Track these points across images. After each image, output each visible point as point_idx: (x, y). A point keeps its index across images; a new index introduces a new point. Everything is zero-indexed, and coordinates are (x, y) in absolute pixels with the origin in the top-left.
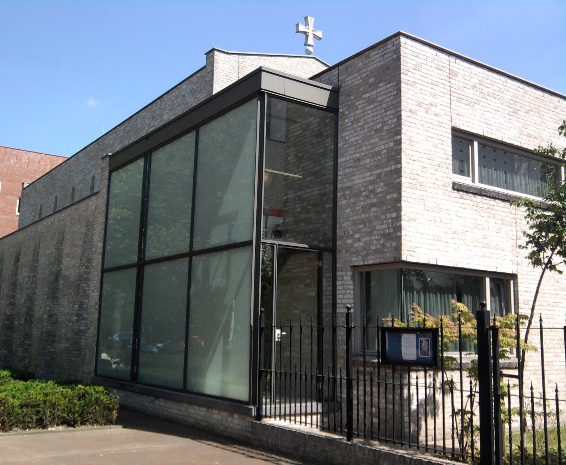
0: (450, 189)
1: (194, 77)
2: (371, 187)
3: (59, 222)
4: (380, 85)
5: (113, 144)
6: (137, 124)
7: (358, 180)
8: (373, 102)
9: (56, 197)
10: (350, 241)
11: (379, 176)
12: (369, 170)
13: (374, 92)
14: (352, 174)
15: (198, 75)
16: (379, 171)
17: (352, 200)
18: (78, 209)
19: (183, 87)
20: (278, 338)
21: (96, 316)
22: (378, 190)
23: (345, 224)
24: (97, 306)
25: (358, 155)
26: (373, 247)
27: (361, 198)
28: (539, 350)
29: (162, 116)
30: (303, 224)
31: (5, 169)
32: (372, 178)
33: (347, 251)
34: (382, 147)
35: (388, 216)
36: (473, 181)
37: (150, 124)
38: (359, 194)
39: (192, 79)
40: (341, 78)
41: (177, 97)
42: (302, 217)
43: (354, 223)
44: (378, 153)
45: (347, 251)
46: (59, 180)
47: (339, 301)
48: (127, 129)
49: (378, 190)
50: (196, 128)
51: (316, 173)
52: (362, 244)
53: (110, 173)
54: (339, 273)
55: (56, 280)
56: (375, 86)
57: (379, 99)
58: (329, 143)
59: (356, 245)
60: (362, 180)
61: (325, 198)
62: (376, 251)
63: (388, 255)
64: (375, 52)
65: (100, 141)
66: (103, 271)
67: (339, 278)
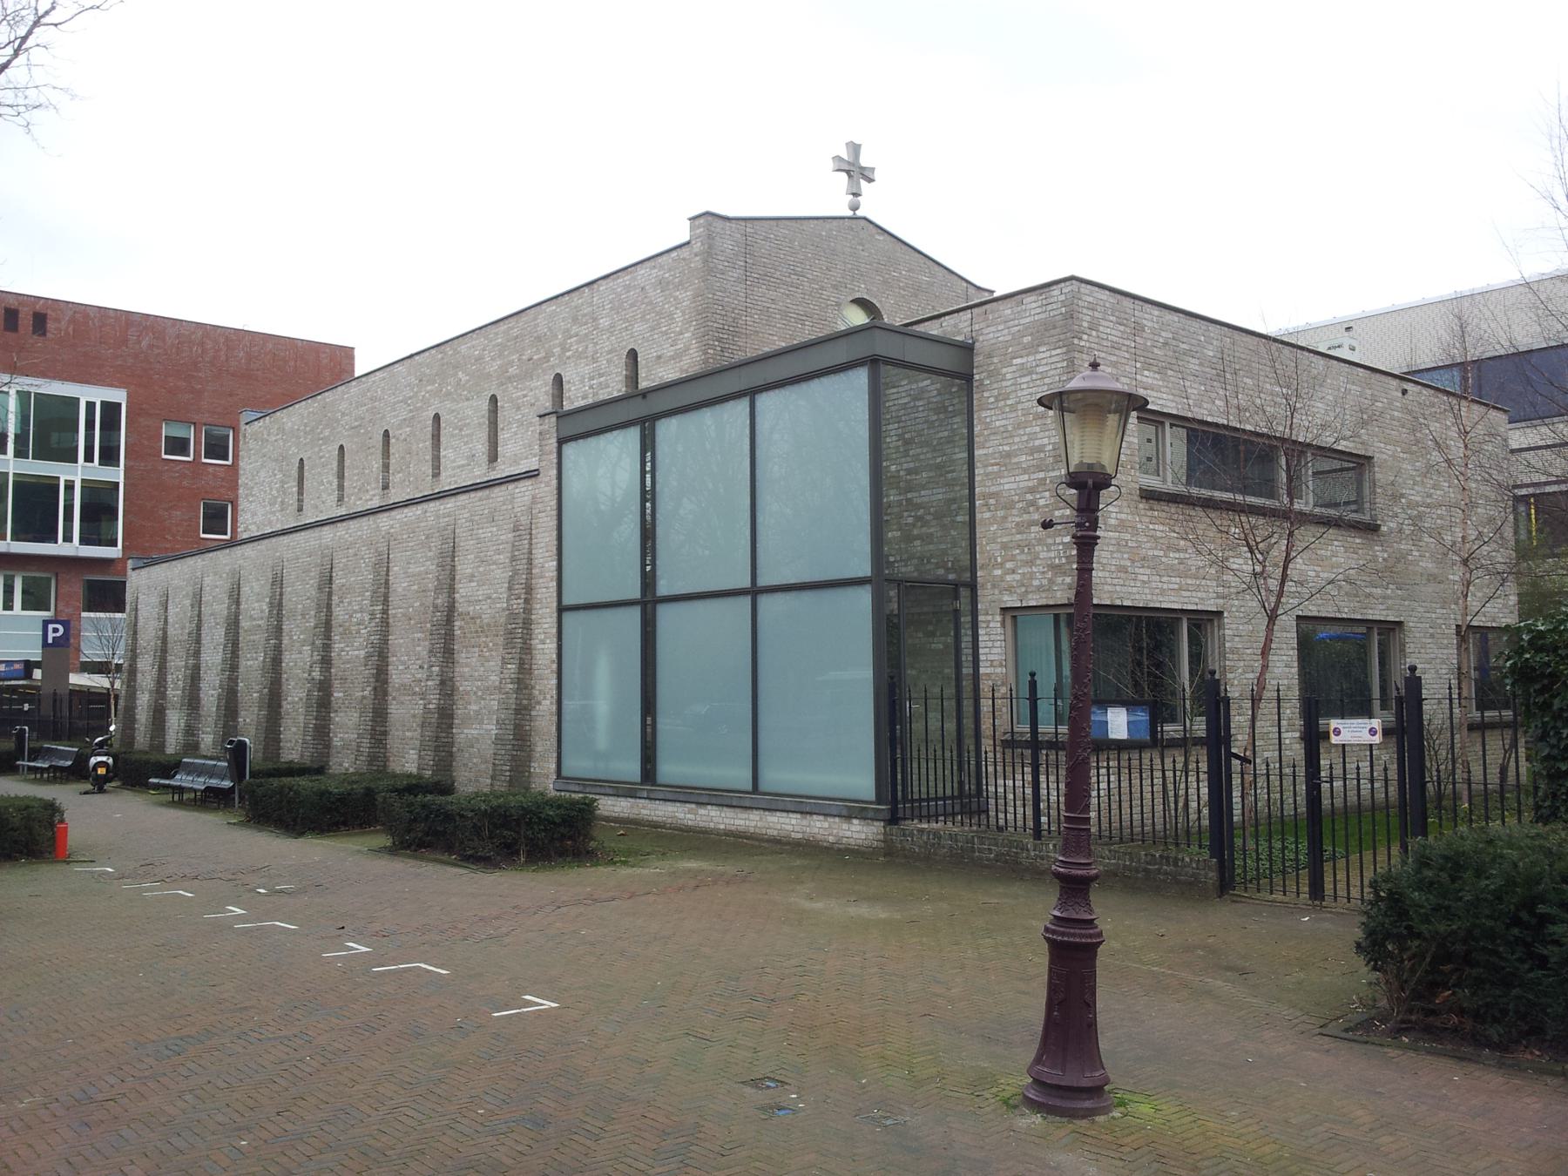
0: (1137, 498)
1: (665, 258)
2: (1029, 497)
3: (438, 517)
4: (1042, 349)
5: (479, 359)
6: (537, 325)
7: (1010, 485)
8: (1030, 373)
9: (341, 447)
10: (998, 572)
11: (1042, 481)
12: (1025, 471)
13: (1031, 358)
14: (999, 475)
15: (674, 254)
16: (1042, 475)
17: (1000, 513)
18: (488, 498)
19: (641, 271)
20: (1058, 720)
21: (554, 682)
22: (1042, 502)
23: (987, 548)
24: (555, 666)
25: (1007, 448)
26: (1036, 583)
27: (1015, 512)
28: (342, 511)
29: (595, 320)
30: (918, 543)
31: (130, 361)
32: (1030, 484)
33: (994, 586)
34: (1046, 441)
35: (1058, 540)
36: (1164, 481)
37: (568, 330)
38: (1010, 506)
39: (660, 260)
40: (976, 327)
41: (628, 288)
42: (915, 532)
43: (1005, 546)
44: (1040, 449)
45: (994, 586)
46: (343, 414)
47: (982, 658)
48: (515, 332)
49: (1042, 502)
50: (752, 393)
51: (939, 467)
52: (1018, 577)
53: (561, 442)
54: (981, 618)
55: (449, 620)
56: (1032, 349)
57: (1040, 369)
58: (958, 422)
59: (1008, 578)
60: (1014, 486)
61: (954, 507)
62: (1039, 589)
63: (1059, 594)
64: (1033, 298)
65: (447, 348)
66: (562, 609)
67: (981, 625)
